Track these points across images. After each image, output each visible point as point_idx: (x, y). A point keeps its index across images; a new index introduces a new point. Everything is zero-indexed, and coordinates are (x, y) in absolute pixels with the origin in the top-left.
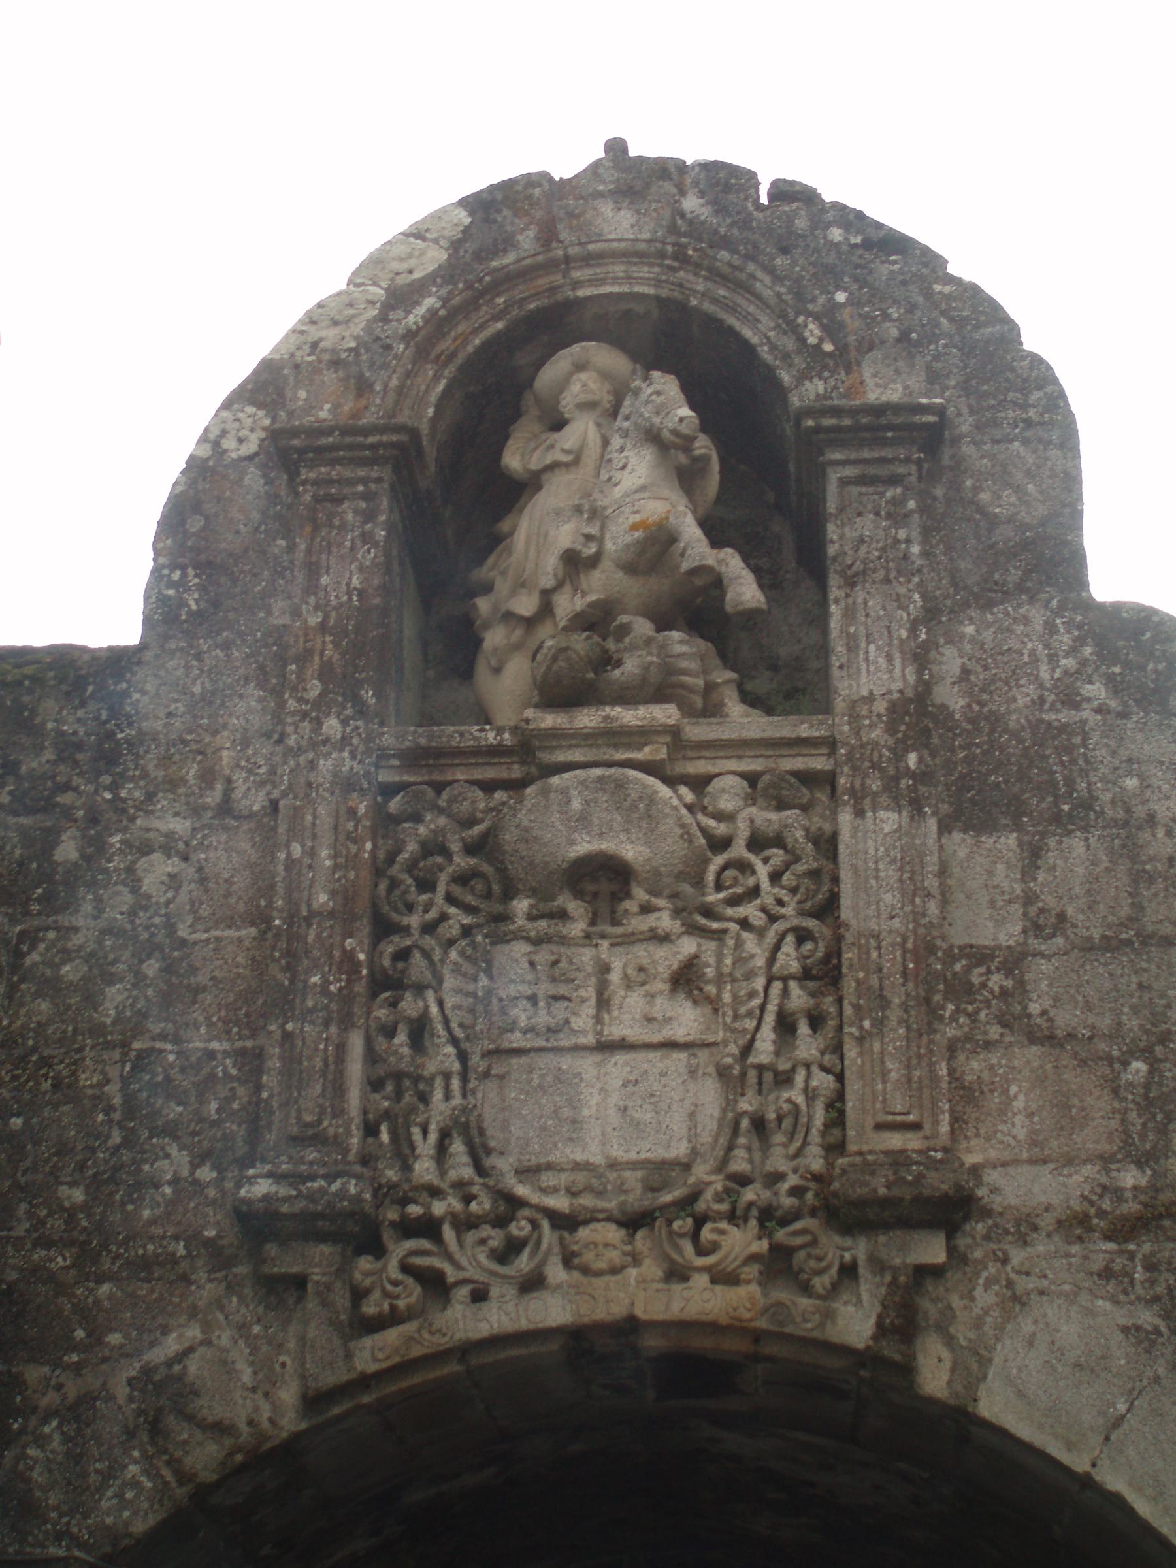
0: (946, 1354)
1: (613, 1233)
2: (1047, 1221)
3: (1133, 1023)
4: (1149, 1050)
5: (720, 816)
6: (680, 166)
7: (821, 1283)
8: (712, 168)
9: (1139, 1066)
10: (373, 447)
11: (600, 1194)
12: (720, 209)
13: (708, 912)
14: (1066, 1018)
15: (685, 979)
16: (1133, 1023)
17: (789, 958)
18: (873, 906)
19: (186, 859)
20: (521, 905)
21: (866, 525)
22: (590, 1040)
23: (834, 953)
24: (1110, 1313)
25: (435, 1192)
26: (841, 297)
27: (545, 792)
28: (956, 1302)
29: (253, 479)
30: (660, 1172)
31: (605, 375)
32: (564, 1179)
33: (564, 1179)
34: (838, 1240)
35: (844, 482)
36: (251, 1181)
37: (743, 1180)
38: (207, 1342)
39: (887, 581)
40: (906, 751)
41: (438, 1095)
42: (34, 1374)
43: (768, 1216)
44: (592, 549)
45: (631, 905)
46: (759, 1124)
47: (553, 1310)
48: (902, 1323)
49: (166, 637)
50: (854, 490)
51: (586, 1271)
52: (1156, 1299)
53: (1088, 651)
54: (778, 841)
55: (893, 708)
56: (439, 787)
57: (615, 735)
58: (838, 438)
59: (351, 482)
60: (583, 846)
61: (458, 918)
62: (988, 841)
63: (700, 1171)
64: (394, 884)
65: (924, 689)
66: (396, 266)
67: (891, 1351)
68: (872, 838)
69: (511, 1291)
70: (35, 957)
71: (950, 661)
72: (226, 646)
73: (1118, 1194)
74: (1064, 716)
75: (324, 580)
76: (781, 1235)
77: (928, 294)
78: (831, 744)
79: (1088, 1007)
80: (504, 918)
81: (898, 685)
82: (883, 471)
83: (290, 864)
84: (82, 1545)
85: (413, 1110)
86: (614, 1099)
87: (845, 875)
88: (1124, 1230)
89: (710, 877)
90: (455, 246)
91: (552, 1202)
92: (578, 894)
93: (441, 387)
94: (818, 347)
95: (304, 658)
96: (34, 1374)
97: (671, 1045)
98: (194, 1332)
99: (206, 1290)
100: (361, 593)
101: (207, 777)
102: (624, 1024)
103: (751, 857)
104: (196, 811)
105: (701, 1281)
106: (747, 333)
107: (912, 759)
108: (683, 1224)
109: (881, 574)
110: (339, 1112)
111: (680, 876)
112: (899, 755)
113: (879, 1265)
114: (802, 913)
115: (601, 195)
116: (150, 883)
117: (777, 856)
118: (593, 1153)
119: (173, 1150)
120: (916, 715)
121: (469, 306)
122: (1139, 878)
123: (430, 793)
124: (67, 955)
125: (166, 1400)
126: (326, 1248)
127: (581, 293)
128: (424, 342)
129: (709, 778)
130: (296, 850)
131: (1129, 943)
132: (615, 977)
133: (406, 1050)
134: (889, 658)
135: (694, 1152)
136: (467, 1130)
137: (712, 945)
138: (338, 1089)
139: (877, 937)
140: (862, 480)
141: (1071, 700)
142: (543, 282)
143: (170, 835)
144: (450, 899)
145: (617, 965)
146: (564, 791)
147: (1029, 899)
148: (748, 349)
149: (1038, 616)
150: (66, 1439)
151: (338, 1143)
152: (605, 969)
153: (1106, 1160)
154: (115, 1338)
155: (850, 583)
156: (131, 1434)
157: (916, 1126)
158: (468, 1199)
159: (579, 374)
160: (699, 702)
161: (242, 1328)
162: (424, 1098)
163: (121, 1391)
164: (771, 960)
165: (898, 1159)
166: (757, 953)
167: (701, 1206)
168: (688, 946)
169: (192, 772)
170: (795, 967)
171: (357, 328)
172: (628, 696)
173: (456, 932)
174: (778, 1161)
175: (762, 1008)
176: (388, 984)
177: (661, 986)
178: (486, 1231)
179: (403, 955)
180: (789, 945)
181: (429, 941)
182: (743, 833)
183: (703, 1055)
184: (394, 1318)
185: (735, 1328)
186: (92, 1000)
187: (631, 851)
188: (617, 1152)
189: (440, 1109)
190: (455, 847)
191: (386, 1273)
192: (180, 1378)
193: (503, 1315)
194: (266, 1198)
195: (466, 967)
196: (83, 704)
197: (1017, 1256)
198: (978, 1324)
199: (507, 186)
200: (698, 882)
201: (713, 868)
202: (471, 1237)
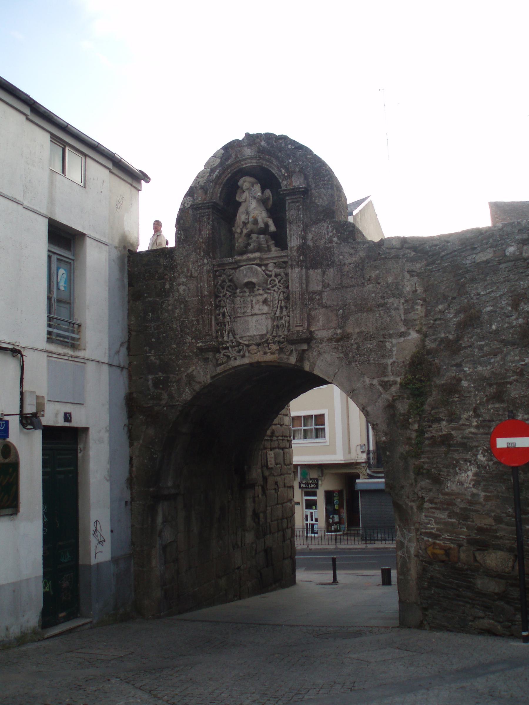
0: (309, 364)
1: (255, 347)
2: (325, 340)
3: (340, 303)
4: (343, 308)
5: (270, 271)
6: (261, 135)
7: (288, 353)
8: (267, 134)
9: (341, 311)
10: (208, 206)
11: (253, 340)
12: (268, 144)
13: (269, 289)
14: (329, 303)
15: (265, 302)
16: (340, 303)
17: (281, 297)
18: (295, 287)
19: (186, 286)
20: (238, 291)
21: (293, 212)
22: (250, 314)
23: (288, 295)
24: (336, 355)
25: (228, 342)
26: (290, 161)
27: (239, 271)
28: (310, 355)
29: (190, 211)
30: (262, 336)
31: (249, 182)
32: (247, 338)
33: (247, 338)
34: (290, 346)
35: (289, 203)
36: (198, 343)
37: (275, 337)
38: (196, 369)
39: (297, 223)
40: (300, 256)
41: (227, 325)
42: (171, 376)
43: (279, 342)
44: (247, 221)
45: (255, 289)
46: (277, 326)
47: (246, 361)
48: (301, 358)
49: (179, 244)
50: (291, 204)
51: (251, 354)
52: (343, 352)
53: (334, 231)
54: (280, 275)
55: (298, 248)
56: (224, 270)
57: (250, 259)
58: (288, 195)
59: (205, 213)
60: (246, 280)
61: (229, 294)
62: (316, 271)
63: (268, 336)
64: (218, 289)
65: (304, 244)
66: (211, 164)
67: (298, 364)
68: (295, 273)
69: (240, 358)
70: (164, 306)
71: (310, 236)
72: (189, 245)
73: (337, 334)
74: (330, 245)
75: (202, 233)
76: (281, 346)
77: (306, 158)
78: (287, 256)
79: (333, 301)
80: (236, 293)
81: (298, 244)
82: (296, 200)
83: (201, 287)
84: (181, 402)
85: (223, 328)
86: (254, 324)
87: (290, 281)
88: (338, 340)
89: (269, 283)
90: (221, 158)
91: (245, 343)
92: (247, 288)
93: (220, 189)
94: (284, 175)
95: (200, 248)
96: (171, 376)
97: (263, 314)
98: (194, 367)
99: (195, 360)
100: (208, 234)
101: (188, 270)
102: (256, 311)
103: (275, 278)
104: (187, 277)
105: (269, 354)
106: (273, 171)
107: (301, 257)
108: (266, 345)
109: (295, 222)
110: (211, 330)
111: (264, 283)
112: (299, 257)
113: (296, 350)
114: (284, 288)
115: (245, 146)
116: (181, 291)
117: (279, 277)
118: (251, 333)
119: (188, 337)
120: (303, 249)
121: (223, 172)
122: (342, 275)
123: (223, 271)
124: (169, 305)
125: (191, 378)
126: (211, 353)
127: (244, 166)
128: (216, 182)
129: (268, 264)
130: (202, 284)
131: (340, 288)
132: (254, 302)
133: (221, 318)
134: (297, 238)
135: (267, 332)
136: (233, 332)
137: (269, 295)
138: (211, 326)
139: (295, 292)
140: (293, 202)
141: (331, 242)
142: (236, 165)
143: (183, 282)
144: (227, 290)
145: (254, 300)
146: (243, 270)
147: (323, 281)
148: (273, 174)
149: (325, 225)
150: (177, 386)
151: (212, 335)
152: (252, 301)
153: (335, 328)
154: (182, 369)
155: (290, 223)
156: (186, 384)
157: (302, 326)
158: (233, 343)
159: (245, 182)
160: (266, 249)
161: (201, 366)
162: (225, 326)
163: (184, 377)
164: (279, 297)
165: (298, 332)
166: (276, 296)
167: (268, 342)
168: (265, 296)
169: (185, 270)
170: (282, 298)
171: (206, 178)
172: (252, 252)
173: (228, 296)
174: (280, 333)
175: (278, 306)
176: (218, 306)
177: (261, 303)
178: (236, 348)
179: (220, 301)
180: (281, 295)
181: (225, 299)
182: (273, 274)
183: (268, 315)
184: (223, 363)
185: (274, 362)
186: (174, 313)
187: (254, 280)
188: (255, 333)
189: (228, 327)
190: (227, 281)
191: (221, 356)
192: (193, 375)
193: (239, 362)
194: (201, 346)
195: (230, 302)
196: (167, 259)
197: (320, 346)
198: (314, 358)
199: (230, 143)
200: (267, 284)
201: (269, 281)
202: (234, 349)
